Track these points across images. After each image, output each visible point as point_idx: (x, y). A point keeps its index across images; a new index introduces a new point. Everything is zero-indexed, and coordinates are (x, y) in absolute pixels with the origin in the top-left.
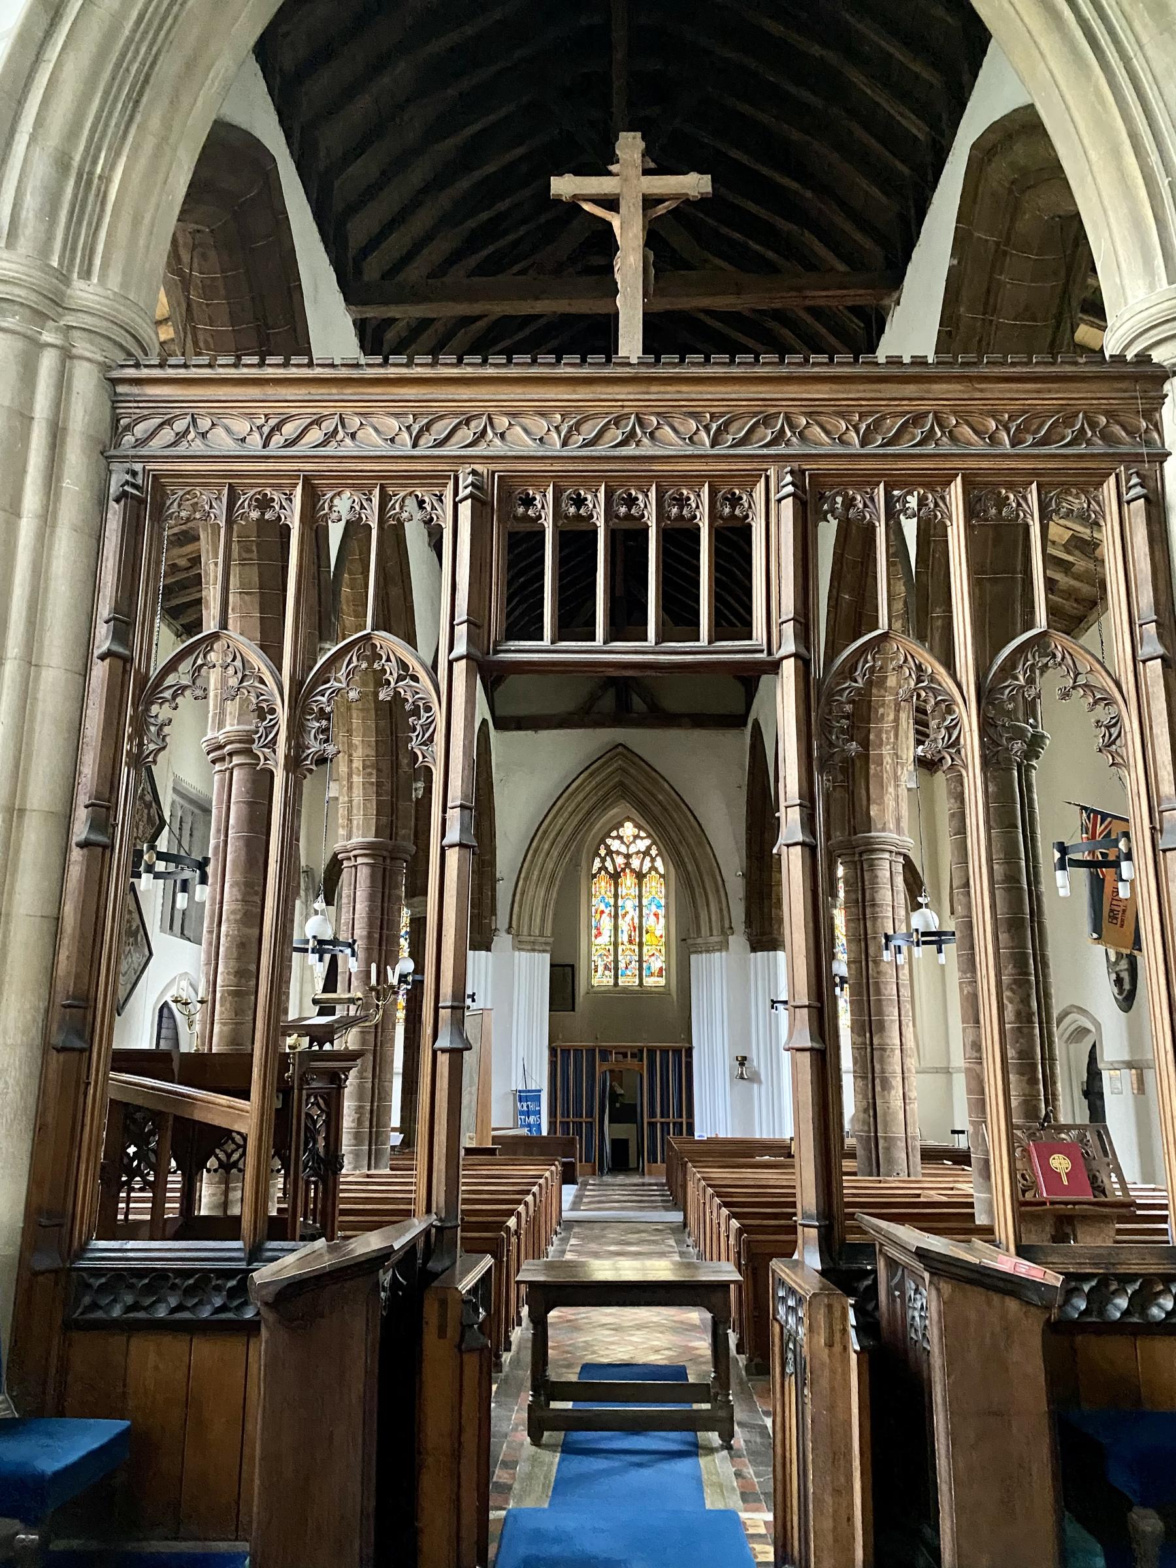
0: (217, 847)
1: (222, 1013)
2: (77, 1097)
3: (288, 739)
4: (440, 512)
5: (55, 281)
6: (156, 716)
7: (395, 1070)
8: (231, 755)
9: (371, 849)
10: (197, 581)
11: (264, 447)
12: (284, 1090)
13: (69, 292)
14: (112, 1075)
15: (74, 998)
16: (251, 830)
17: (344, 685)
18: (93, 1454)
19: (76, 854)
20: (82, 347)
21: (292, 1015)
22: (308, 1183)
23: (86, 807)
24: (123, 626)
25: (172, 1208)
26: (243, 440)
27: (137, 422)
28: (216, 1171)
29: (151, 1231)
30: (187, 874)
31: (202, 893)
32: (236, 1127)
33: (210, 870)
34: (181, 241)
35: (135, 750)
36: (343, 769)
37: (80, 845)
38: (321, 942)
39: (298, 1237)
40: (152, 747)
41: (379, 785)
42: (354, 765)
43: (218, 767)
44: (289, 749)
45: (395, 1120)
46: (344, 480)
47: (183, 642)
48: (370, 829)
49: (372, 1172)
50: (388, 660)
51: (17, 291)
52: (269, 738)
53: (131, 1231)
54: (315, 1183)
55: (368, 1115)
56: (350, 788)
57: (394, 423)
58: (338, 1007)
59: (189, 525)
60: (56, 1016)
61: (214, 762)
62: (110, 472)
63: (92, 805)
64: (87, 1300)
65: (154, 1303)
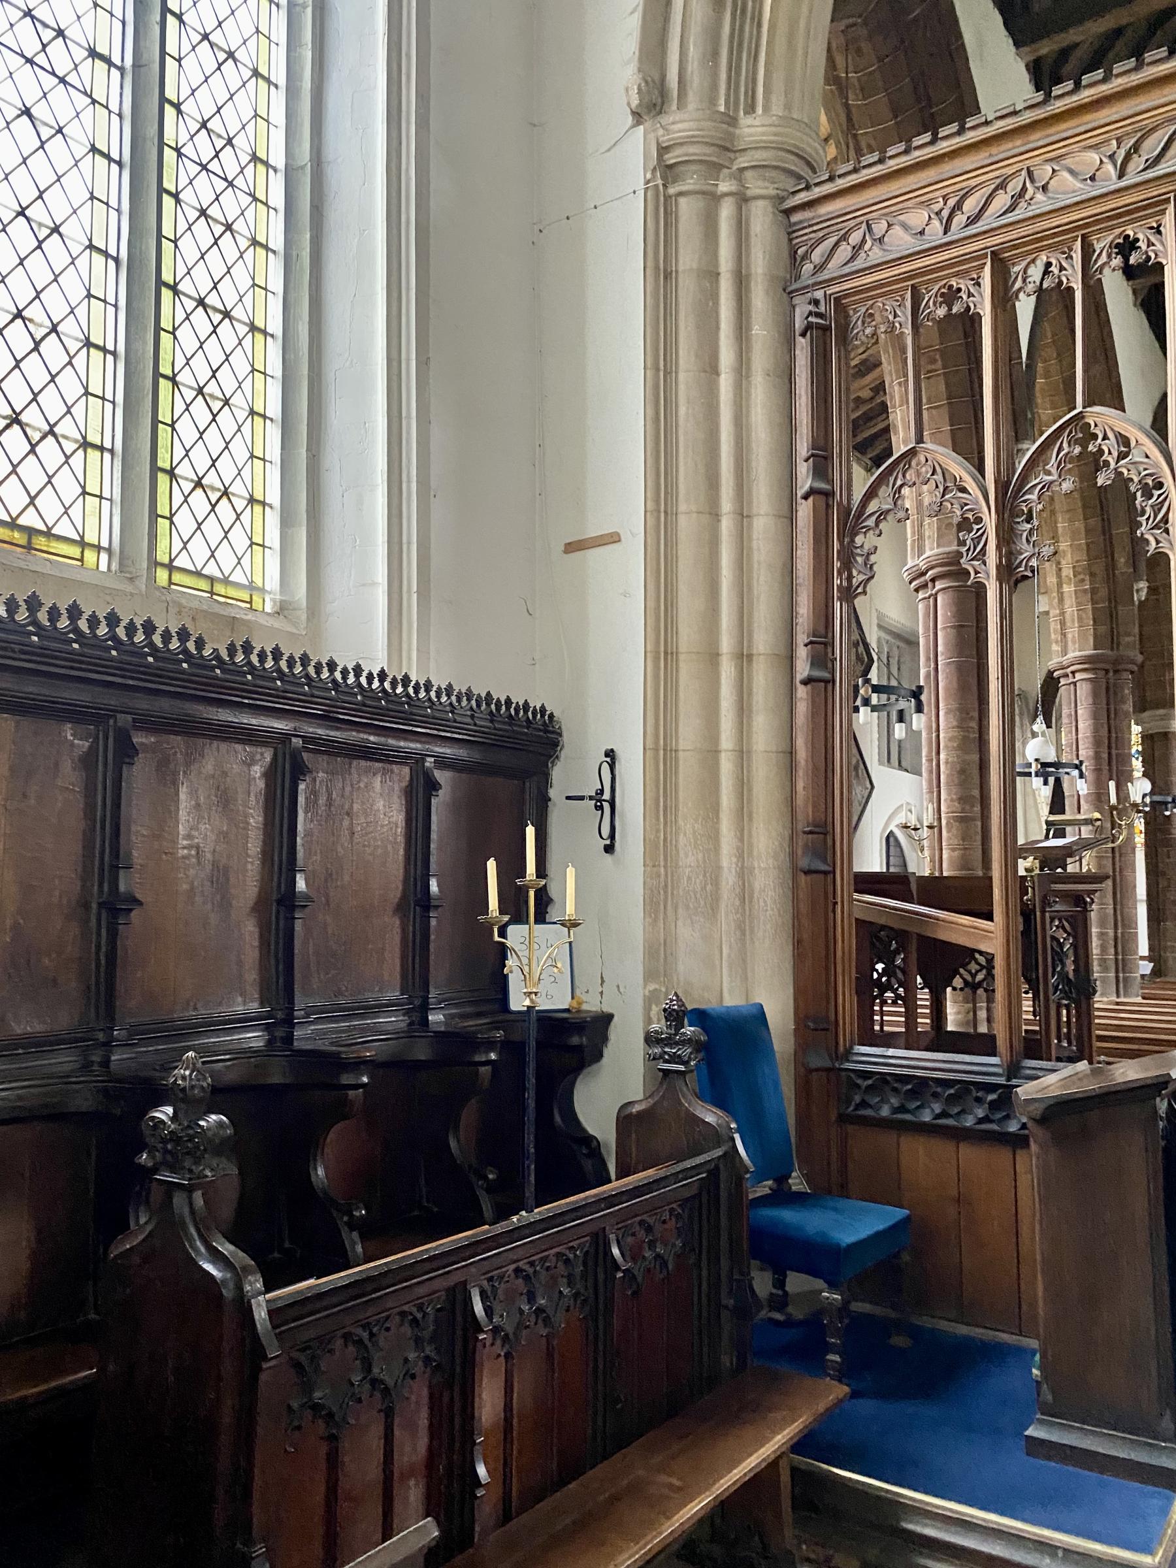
0: (928, 675)
1: (949, 838)
2: (826, 914)
3: (998, 547)
4: (1159, 247)
5: (725, 126)
6: (862, 546)
7: (1139, 897)
8: (933, 580)
9: (1091, 663)
10: (884, 409)
11: (945, 233)
12: (1027, 914)
13: (737, 131)
14: (856, 896)
15: (815, 826)
16: (960, 655)
17: (1055, 477)
18: (878, 1234)
19: (802, 692)
20: (756, 186)
21: (1021, 841)
22: (1059, 1006)
23: (806, 645)
24: (821, 462)
25: (924, 1022)
26: (922, 233)
27: (813, 248)
28: (961, 989)
29: (907, 1041)
30: (902, 704)
31: (918, 722)
32: (983, 948)
33: (923, 698)
34: (834, 45)
35: (845, 584)
36: (1052, 580)
37: (805, 682)
38: (1045, 765)
39: (1054, 1057)
40: (862, 577)
41: (1093, 591)
42: (1064, 574)
43: (921, 595)
44: (1000, 558)
45: (1143, 948)
46: (1038, 243)
47: (872, 475)
48: (1087, 639)
49: (1122, 1000)
50: (1105, 438)
51: (692, 149)
52: (978, 549)
53: (887, 1040)
54: (1068, 1007)
55: (1112, 942)
56: (1061, 600)
57: (1095, 157)
58: (1068, 829)
59: (869, 352)
60: (801, 840)
61: (917, 590)
62: (794, 307)
63: (811, 643)
64: (857, 1099)
65: (918, 1107)
